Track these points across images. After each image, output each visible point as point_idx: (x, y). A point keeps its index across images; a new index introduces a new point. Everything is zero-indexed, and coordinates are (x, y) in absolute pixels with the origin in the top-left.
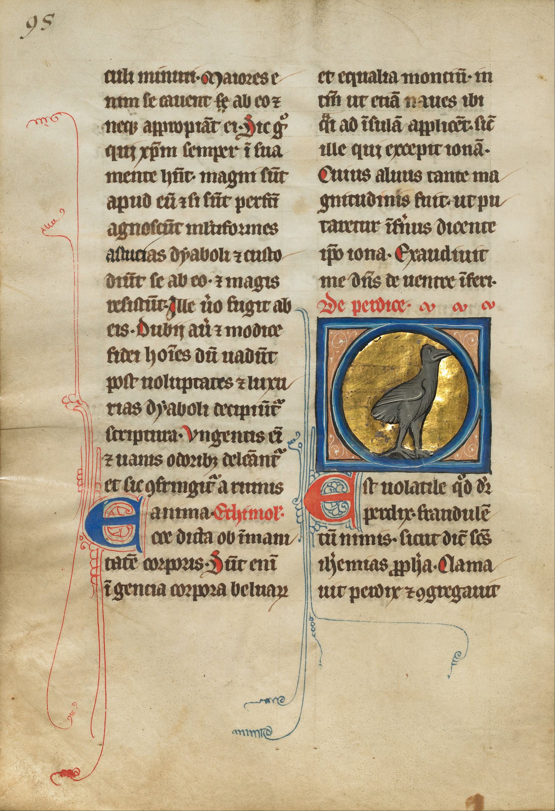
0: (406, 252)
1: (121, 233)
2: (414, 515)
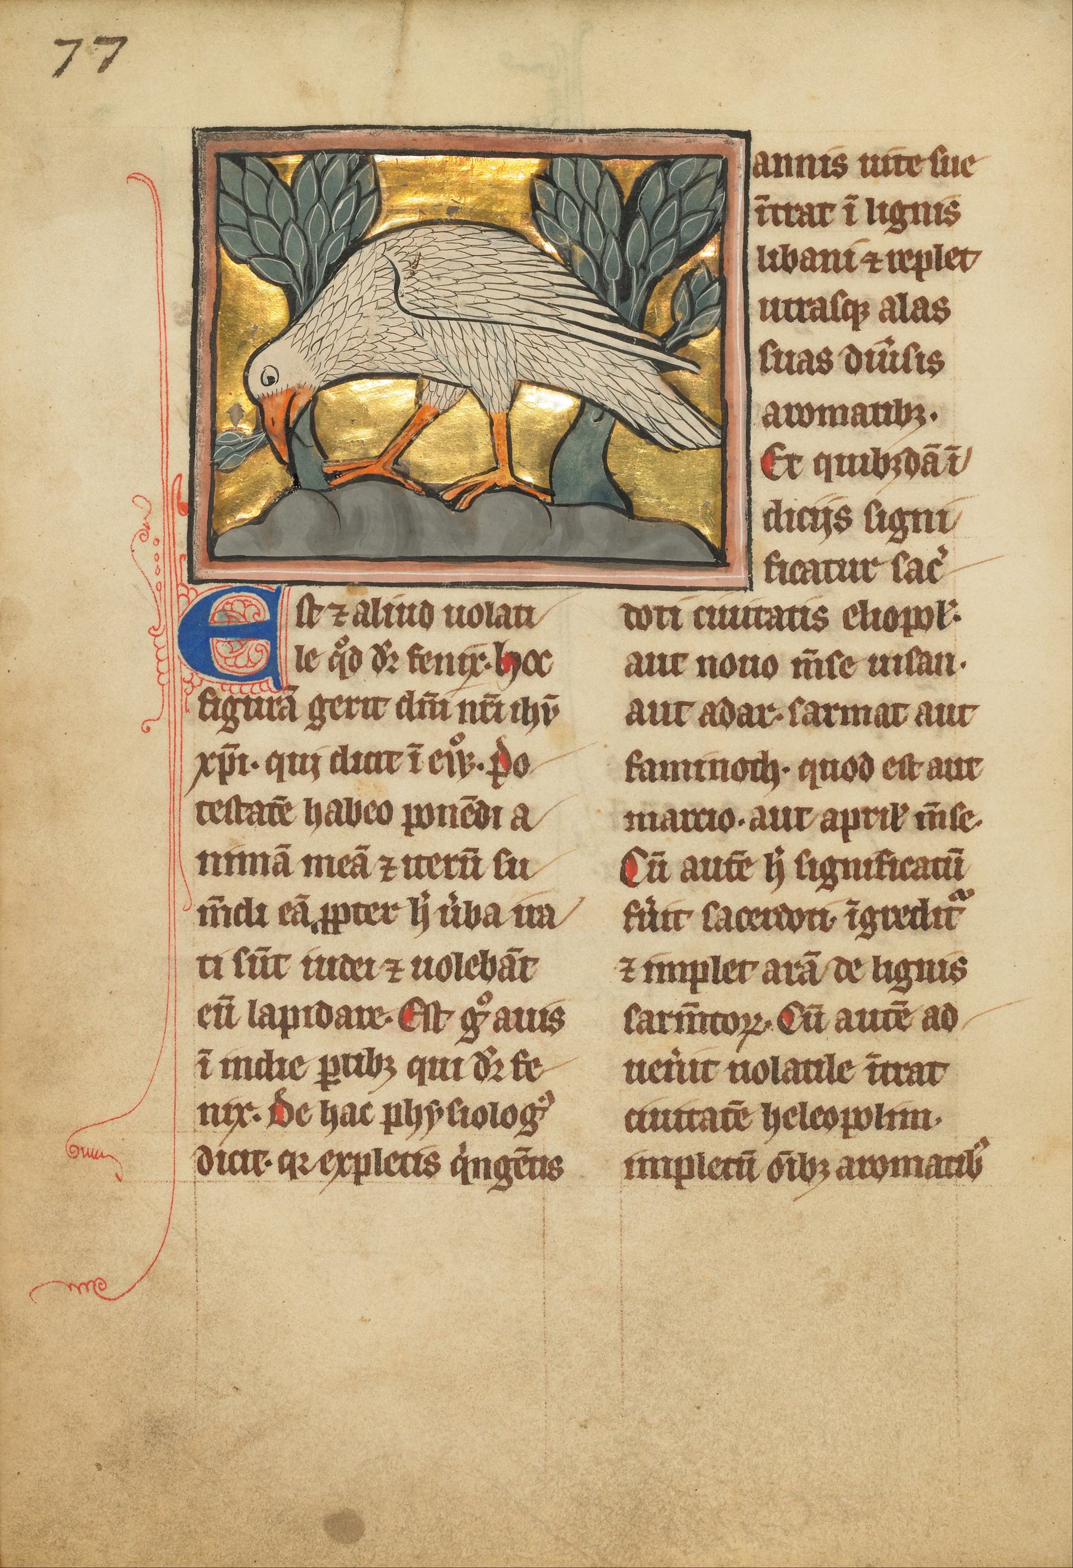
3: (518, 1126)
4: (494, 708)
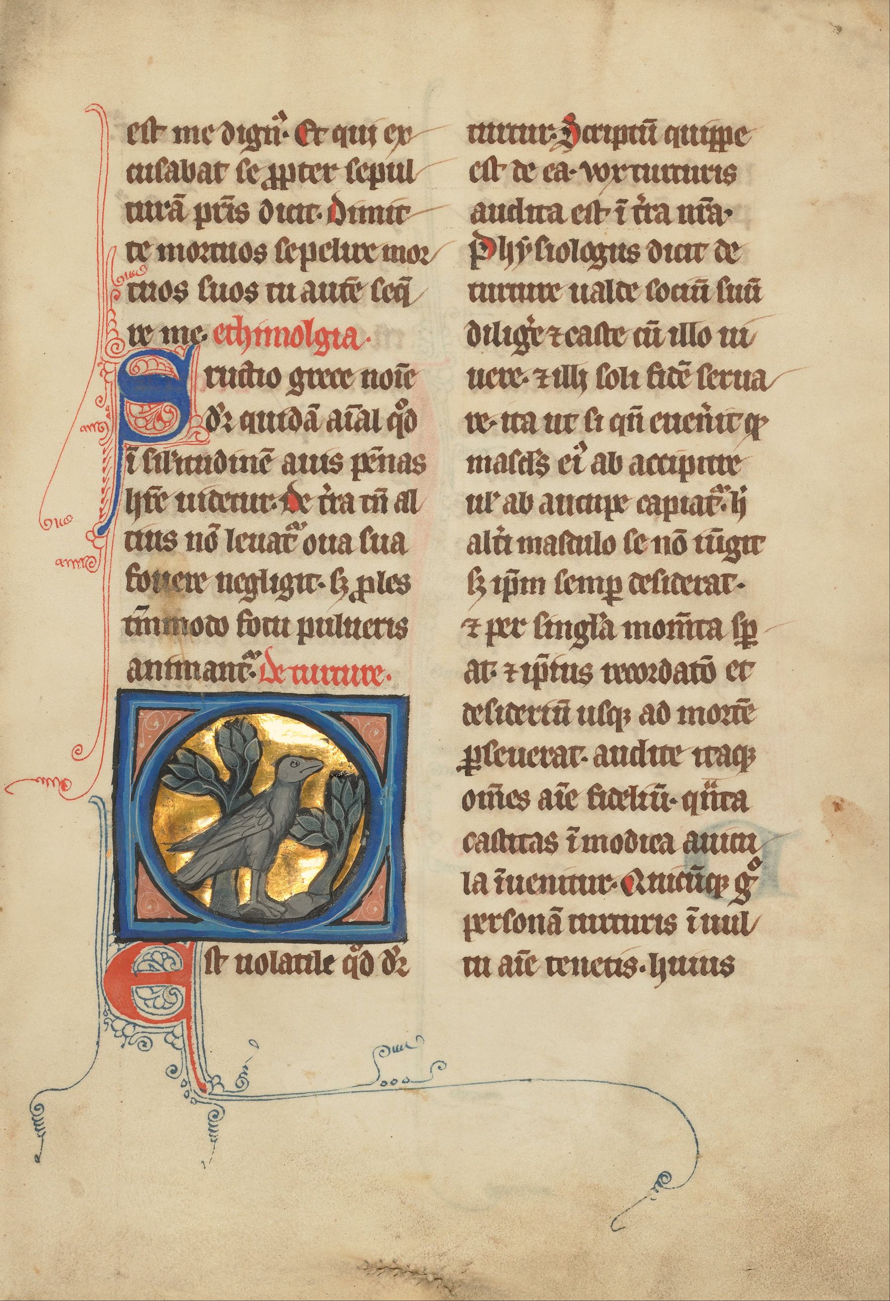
2: (322, 585)
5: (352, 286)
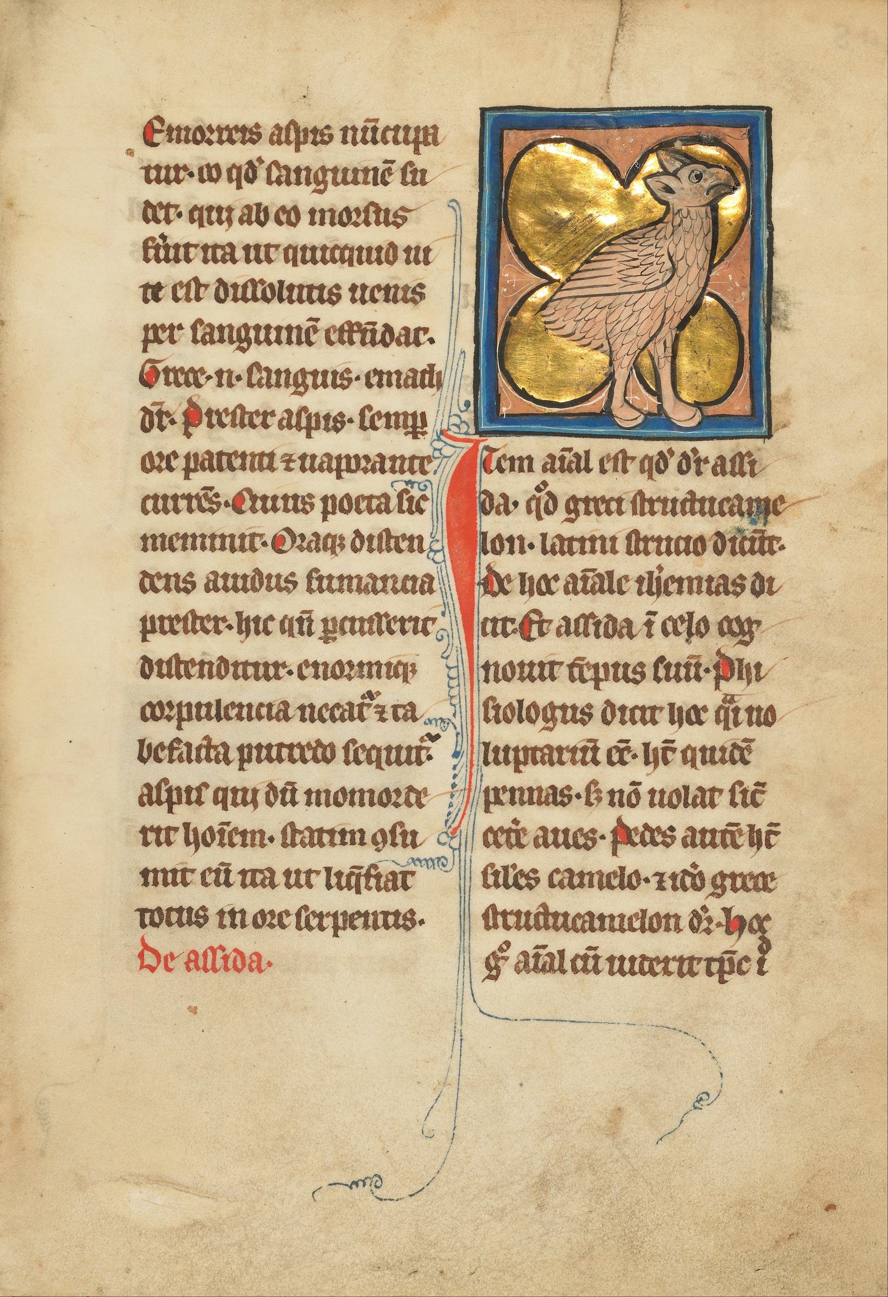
0: (160, 131)
1: (240, 340)
3: (540, 723)
4: (412, 623)
5: (732, 833)
